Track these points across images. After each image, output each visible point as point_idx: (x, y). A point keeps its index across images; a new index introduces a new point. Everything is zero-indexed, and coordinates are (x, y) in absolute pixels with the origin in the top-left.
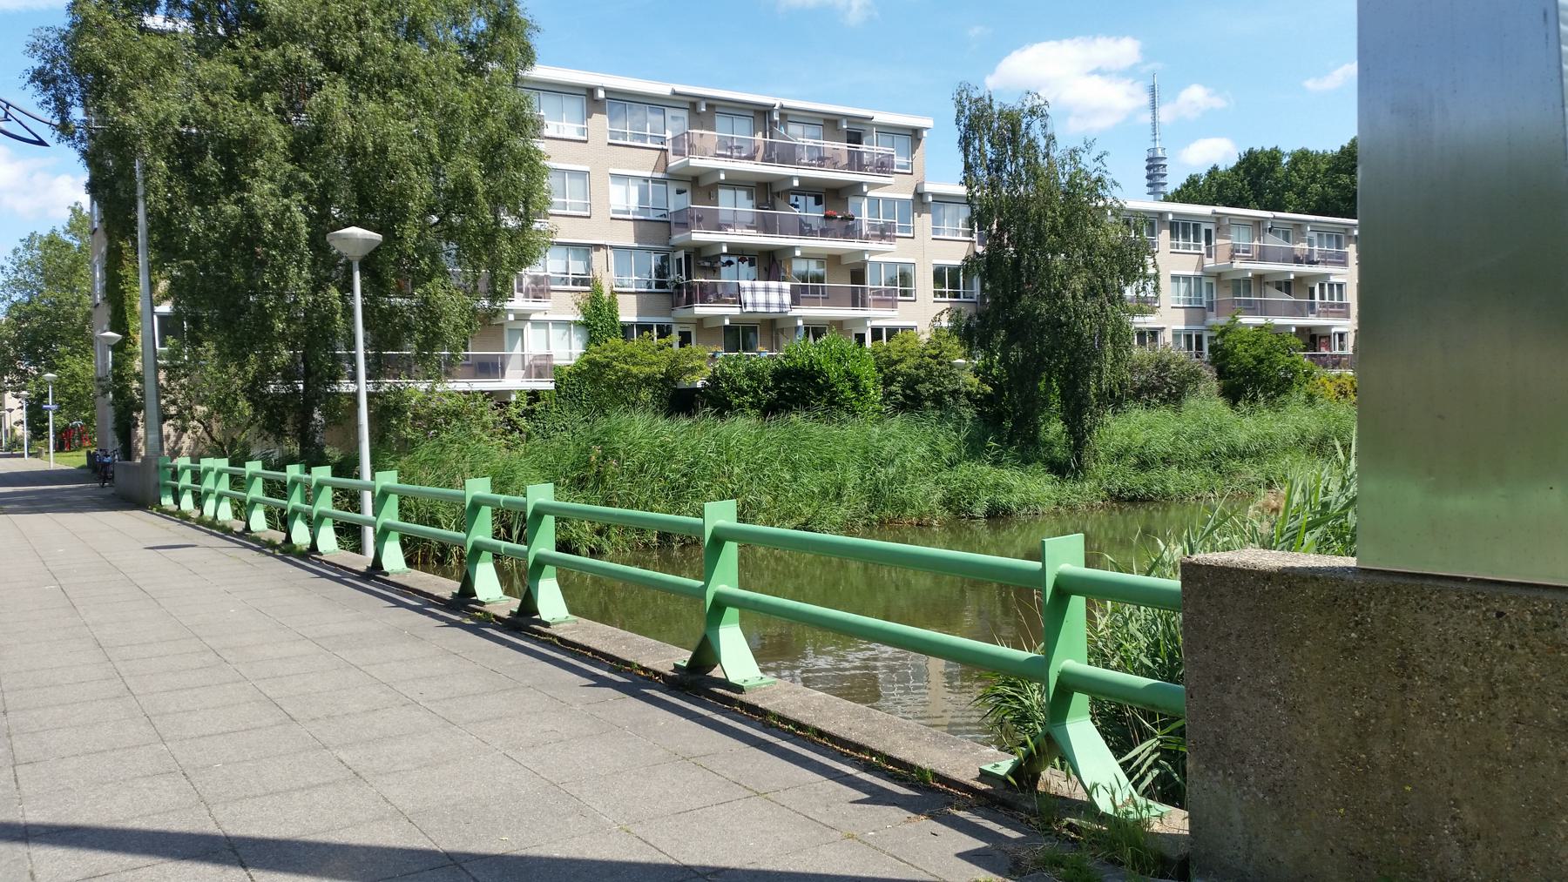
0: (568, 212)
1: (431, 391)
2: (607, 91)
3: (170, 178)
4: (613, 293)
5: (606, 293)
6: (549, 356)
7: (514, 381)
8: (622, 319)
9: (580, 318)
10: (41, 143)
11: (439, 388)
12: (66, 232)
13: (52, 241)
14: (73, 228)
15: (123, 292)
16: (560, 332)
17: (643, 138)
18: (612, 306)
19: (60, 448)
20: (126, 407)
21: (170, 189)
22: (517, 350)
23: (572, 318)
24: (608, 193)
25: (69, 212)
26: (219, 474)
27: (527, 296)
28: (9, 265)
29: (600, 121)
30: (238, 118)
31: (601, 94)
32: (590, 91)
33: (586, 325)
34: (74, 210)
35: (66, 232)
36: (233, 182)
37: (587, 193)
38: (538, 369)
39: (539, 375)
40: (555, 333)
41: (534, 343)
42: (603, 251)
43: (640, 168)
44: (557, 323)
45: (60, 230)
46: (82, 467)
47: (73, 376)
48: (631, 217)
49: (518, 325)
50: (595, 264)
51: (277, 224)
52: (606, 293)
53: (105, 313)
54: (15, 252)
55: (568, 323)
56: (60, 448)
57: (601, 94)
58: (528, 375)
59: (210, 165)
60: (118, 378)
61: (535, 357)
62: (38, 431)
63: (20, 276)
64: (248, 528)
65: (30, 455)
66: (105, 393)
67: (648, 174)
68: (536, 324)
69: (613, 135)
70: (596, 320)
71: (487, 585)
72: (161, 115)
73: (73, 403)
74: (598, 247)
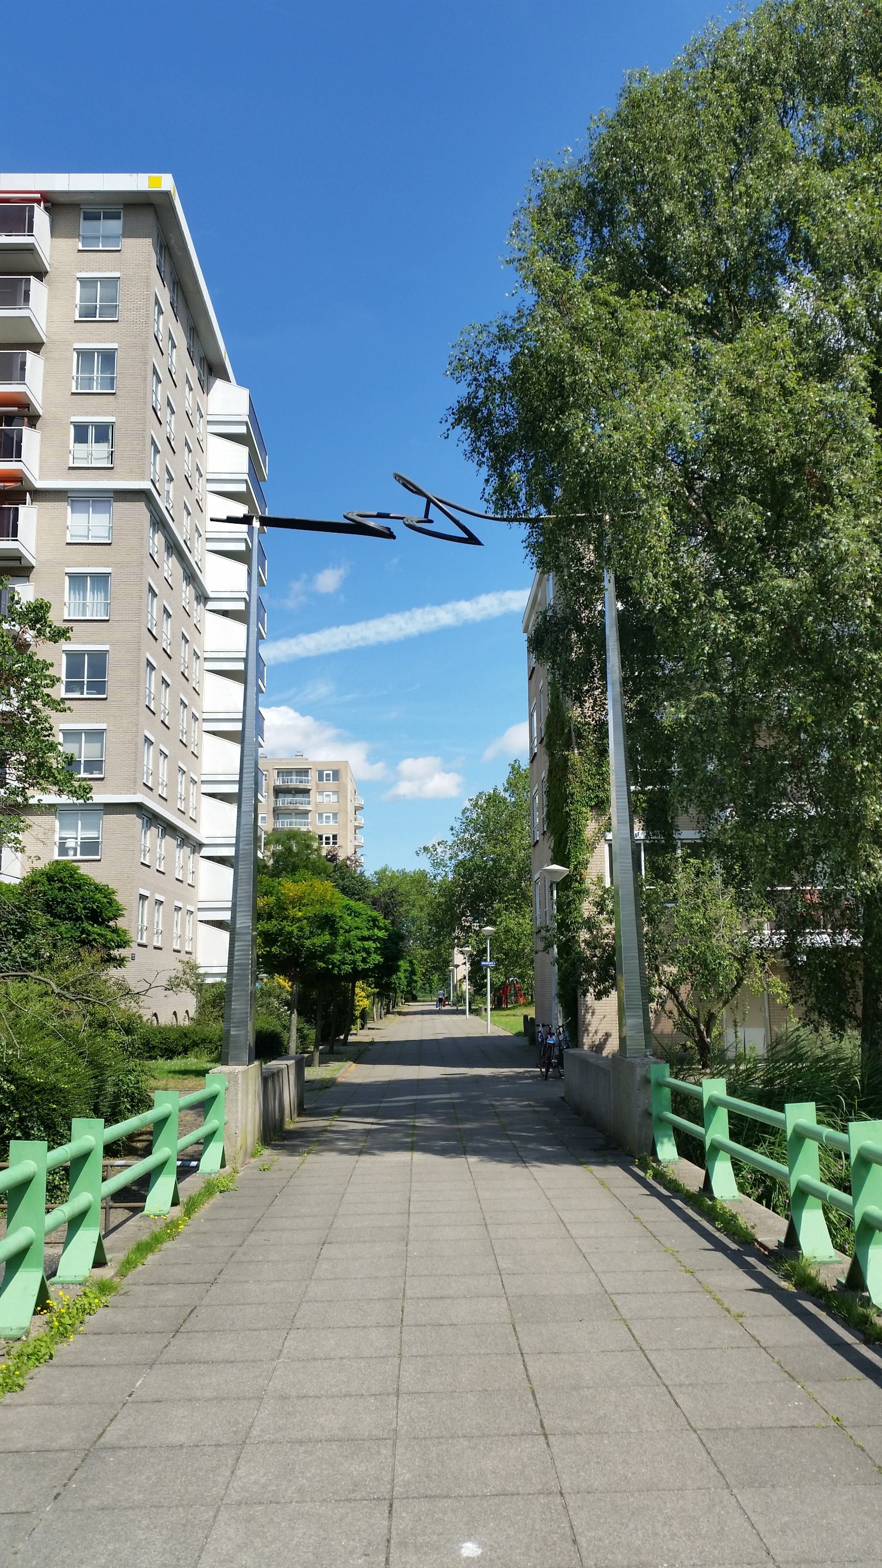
10: (472, 539)
12: (506, 790)
13: (493, 800)
14: (511, 786)
15: (568, 814)
19: (498, 1005)
20: (573, 965)
25: (509, 769)
34: (513, 768)
35: (506, 790)
45: (501, 789)
46: (518, 1034)
47: (508, 931)
53: (547, 846)
56: (498, 1005)
59: (748, 514)
60: (563, 926)
62: (479, 988)
63: (467, 836)
64: (856, 1279)
65: (472, 1011)
66: (548, 946)
71: (816, 1241)
72: (661, 425)
73: (510, 958)
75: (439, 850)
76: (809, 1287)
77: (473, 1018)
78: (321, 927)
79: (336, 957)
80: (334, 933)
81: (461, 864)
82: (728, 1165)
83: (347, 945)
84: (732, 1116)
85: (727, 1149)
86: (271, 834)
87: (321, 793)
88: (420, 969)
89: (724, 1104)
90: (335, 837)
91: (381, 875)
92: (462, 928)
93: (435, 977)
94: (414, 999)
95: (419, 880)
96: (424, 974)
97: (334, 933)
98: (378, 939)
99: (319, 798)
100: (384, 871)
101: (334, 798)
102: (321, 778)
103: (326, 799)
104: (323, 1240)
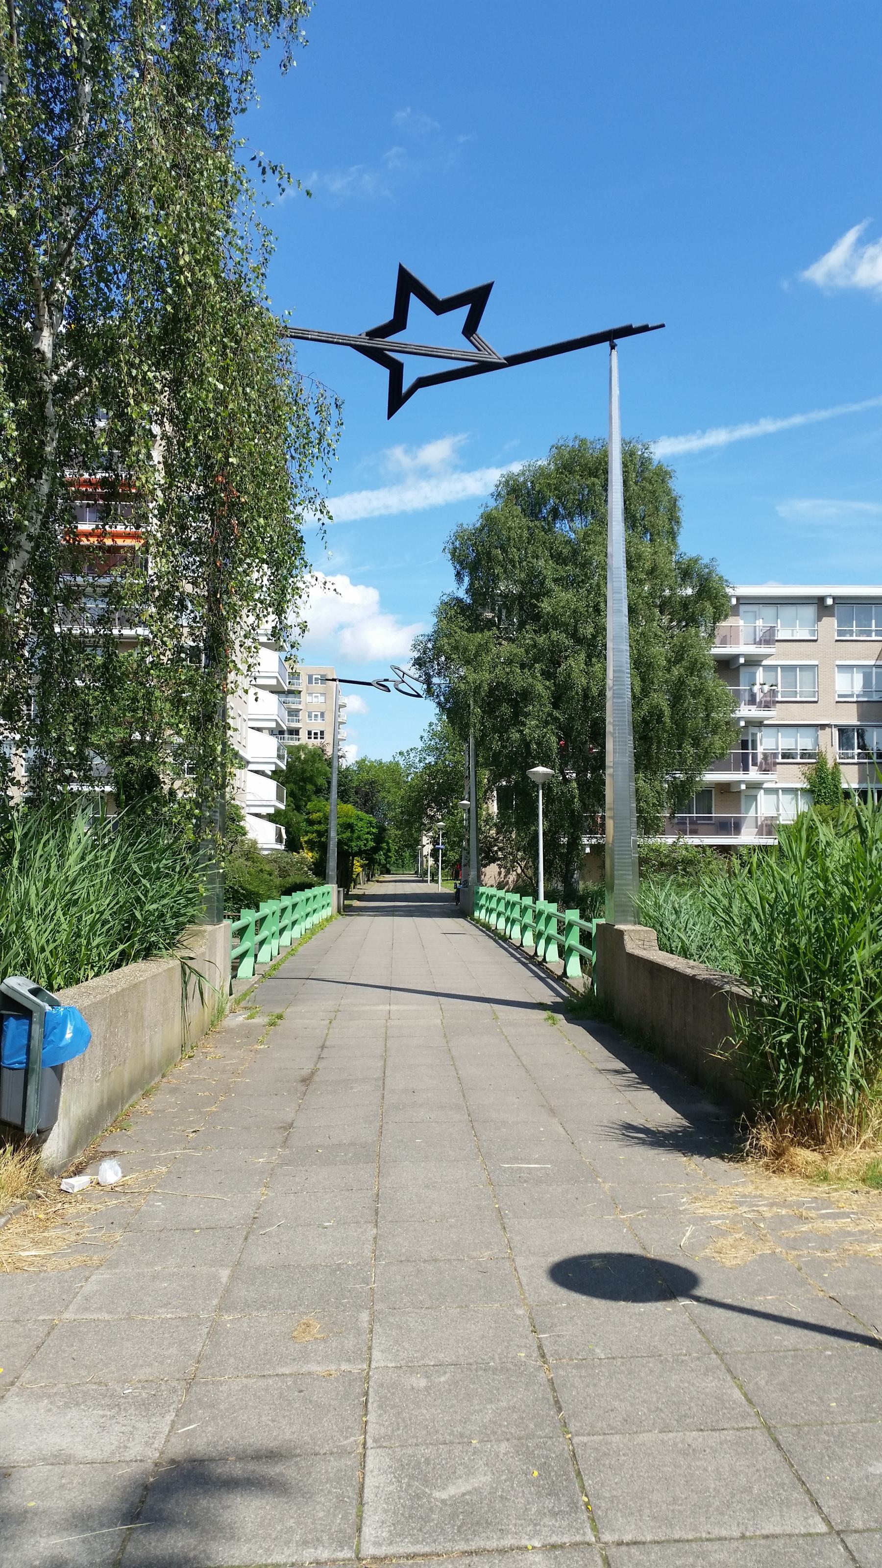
0: (798, 699)
1: (674, 844)
2: (834, 598)
3: (483, 718)
4: (836, 765)
5: (830, 764)
6: (777, 818)
7: (747, 837)
8: (844, 786)
9: (806, 785)
10: (419, 696)
11: (682, 842)
16: (789, 797)
17: (869, 633)
18: (835, 774)
21: (483, 724)
22: (752, 813)
23: (799, 786)
24: (833, 681)
26: (549, 918)
27: (760, 769)
28: (425, 735)
29: (830, 624)
30: (520, 680)
31: (830, 602)
32: (821, 599)
33: (811, 791)
36: (517, 719)
37: (815, 682)
38: (769, 827)
39: (769, 833)
40: (785, 799)
41: (764, 807)
42: (828, 730)
43: (865, 658)
44: (786, 791)
48: (855, 699)
49: (752, 792)
50: (821, 741)
51: (539, 744)
52: (830, 764)
54: (431, 724)
55: (797, 790)
57: (830, 602)
58: (760, 833)
59: (506, 709)
61: (766, 818)
67: (872, 663)
68: (769, 791)
69: (840, 633)
70: (822, 788)
74: (823, 727)
75: (412, 755)
76: (549, 973)
77: (433, 884)
78: (346, 829)
79: (353, 844)
80: (353, 832)
81: (428, 766)
82: (578, 958)
83: (359, 838)
84: (581, 930)
85: (577, 950)
86: (224, 699)
87: (310, 694)
88: (394, 847)
89: (578, 924)
90: (322, 733)
91: (361, 764)
92: (428, 816)
93: (407, 854)
94: (388, 872)
95: (392, 769)
96: (397, 851)
97: (353, 832)
98: (373, 833)
99: (309, 699)
100: (363, 761)
101: (321, 699)
102: (310, 682)
103: (315, 700)
104: (320, 1044)
